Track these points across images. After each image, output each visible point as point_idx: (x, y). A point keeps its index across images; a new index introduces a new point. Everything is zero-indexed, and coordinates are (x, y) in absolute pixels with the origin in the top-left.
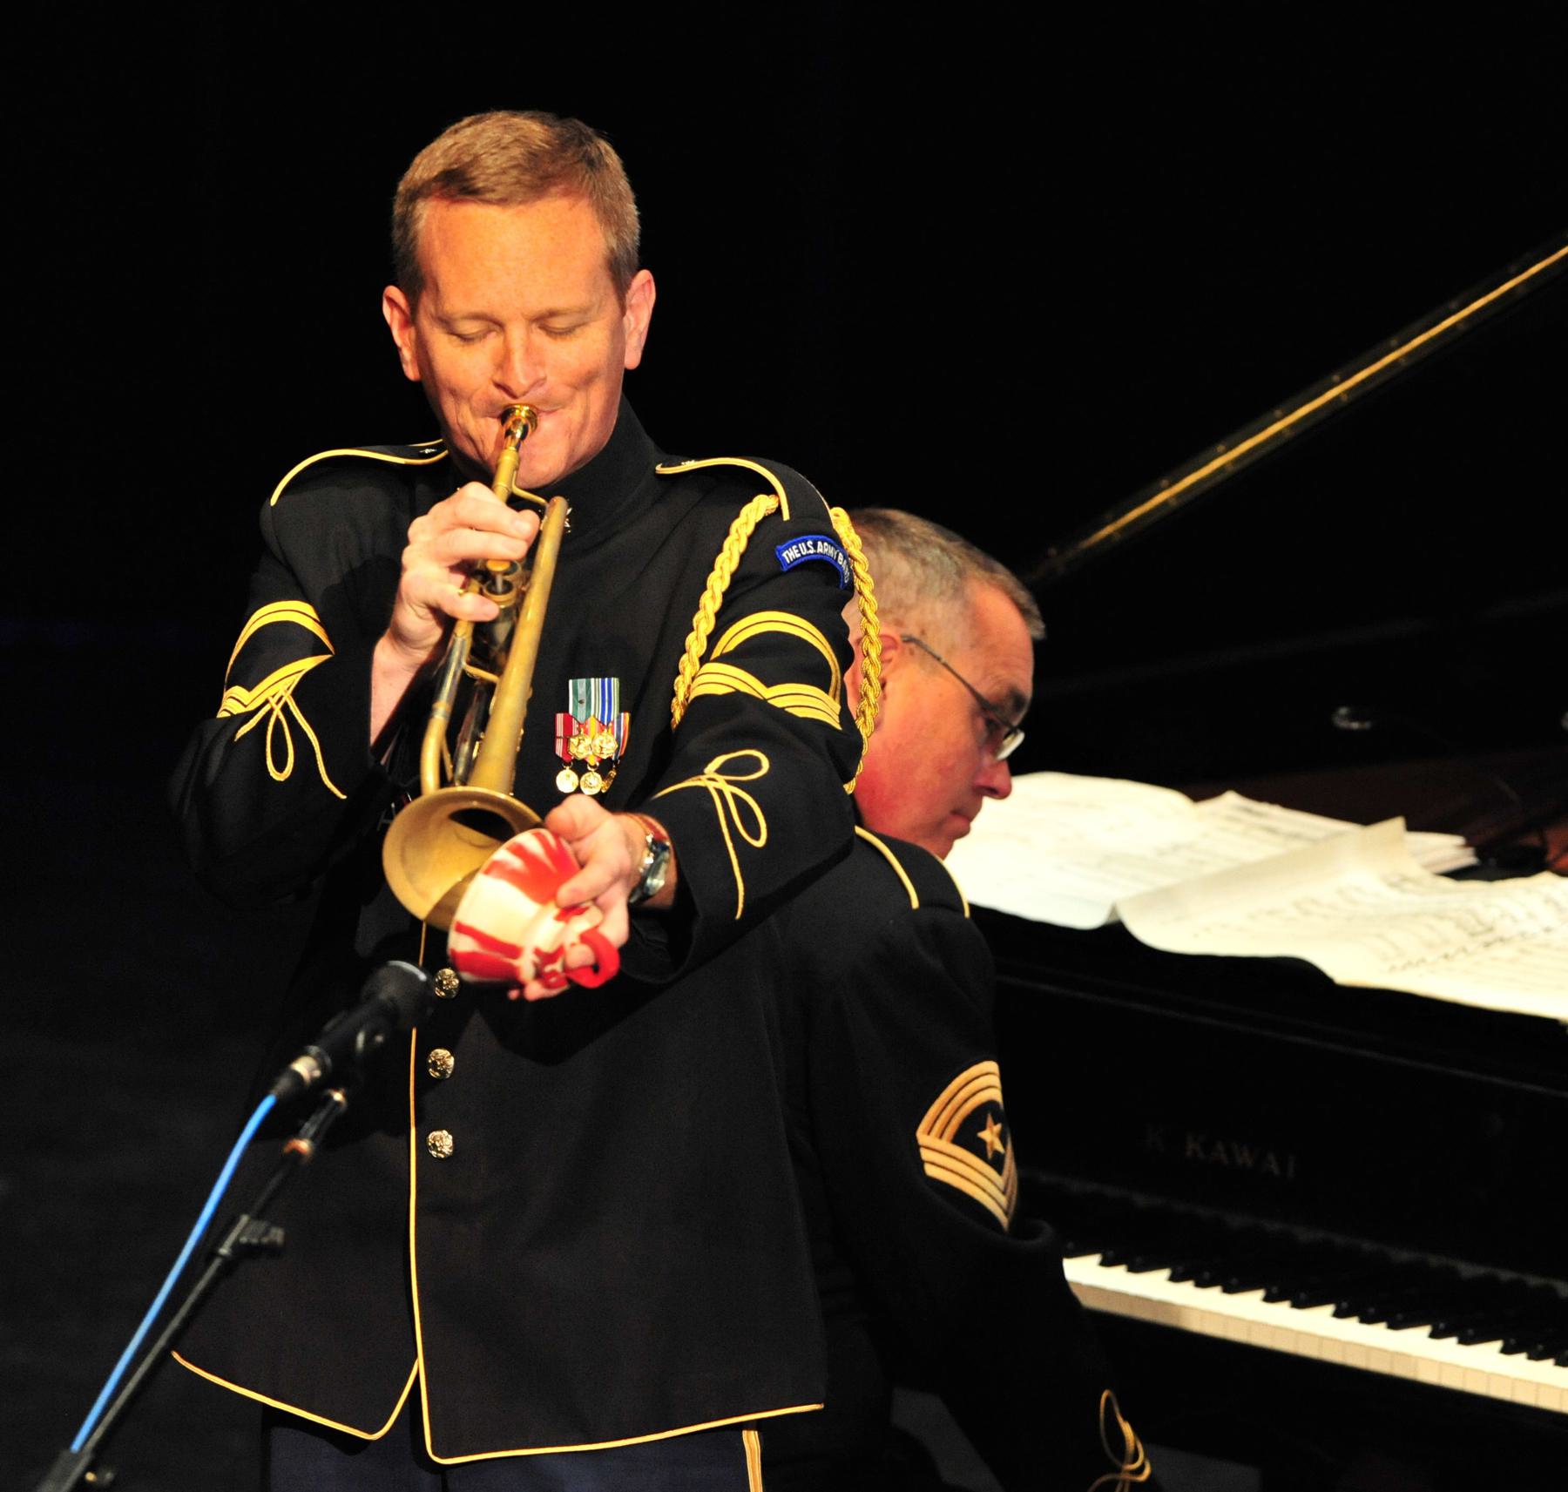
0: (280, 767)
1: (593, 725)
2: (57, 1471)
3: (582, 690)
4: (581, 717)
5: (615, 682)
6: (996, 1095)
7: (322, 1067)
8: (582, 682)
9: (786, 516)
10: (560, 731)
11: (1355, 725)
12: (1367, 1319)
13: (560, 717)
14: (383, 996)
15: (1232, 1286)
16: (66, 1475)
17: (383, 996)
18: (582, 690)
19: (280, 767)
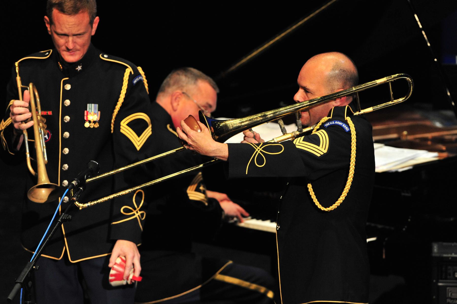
0: (316, 141)
1: (92, 113)
2: (27, 266)
3: (90, 107)
4: (90, 111)
5: (97, 105)
6: (201, 179)
7: (78, 182)
8: (90, 104)
9: (133, 73)
10: (85, 114)
11: (401, 100)
12: (258, 219)
13: (86, 112)
14: (90, 168)
15: (264, 219)
16: (29, 267)
17: (90, 168)
18: (90, 107)
19: (316, 141)
